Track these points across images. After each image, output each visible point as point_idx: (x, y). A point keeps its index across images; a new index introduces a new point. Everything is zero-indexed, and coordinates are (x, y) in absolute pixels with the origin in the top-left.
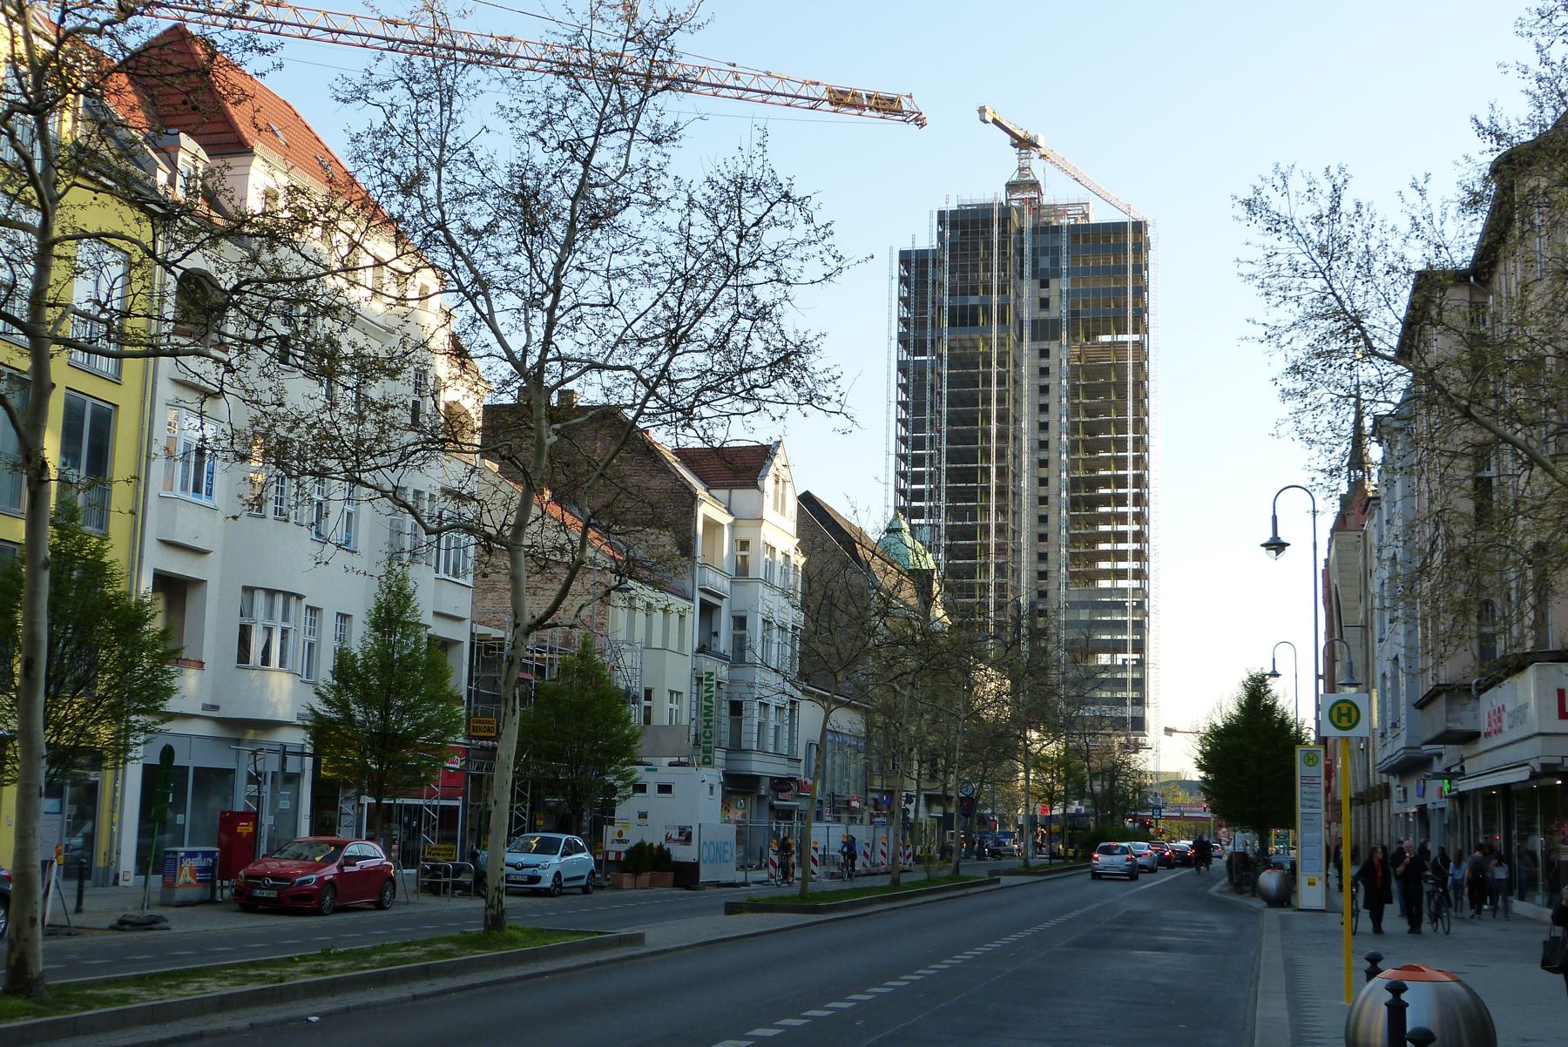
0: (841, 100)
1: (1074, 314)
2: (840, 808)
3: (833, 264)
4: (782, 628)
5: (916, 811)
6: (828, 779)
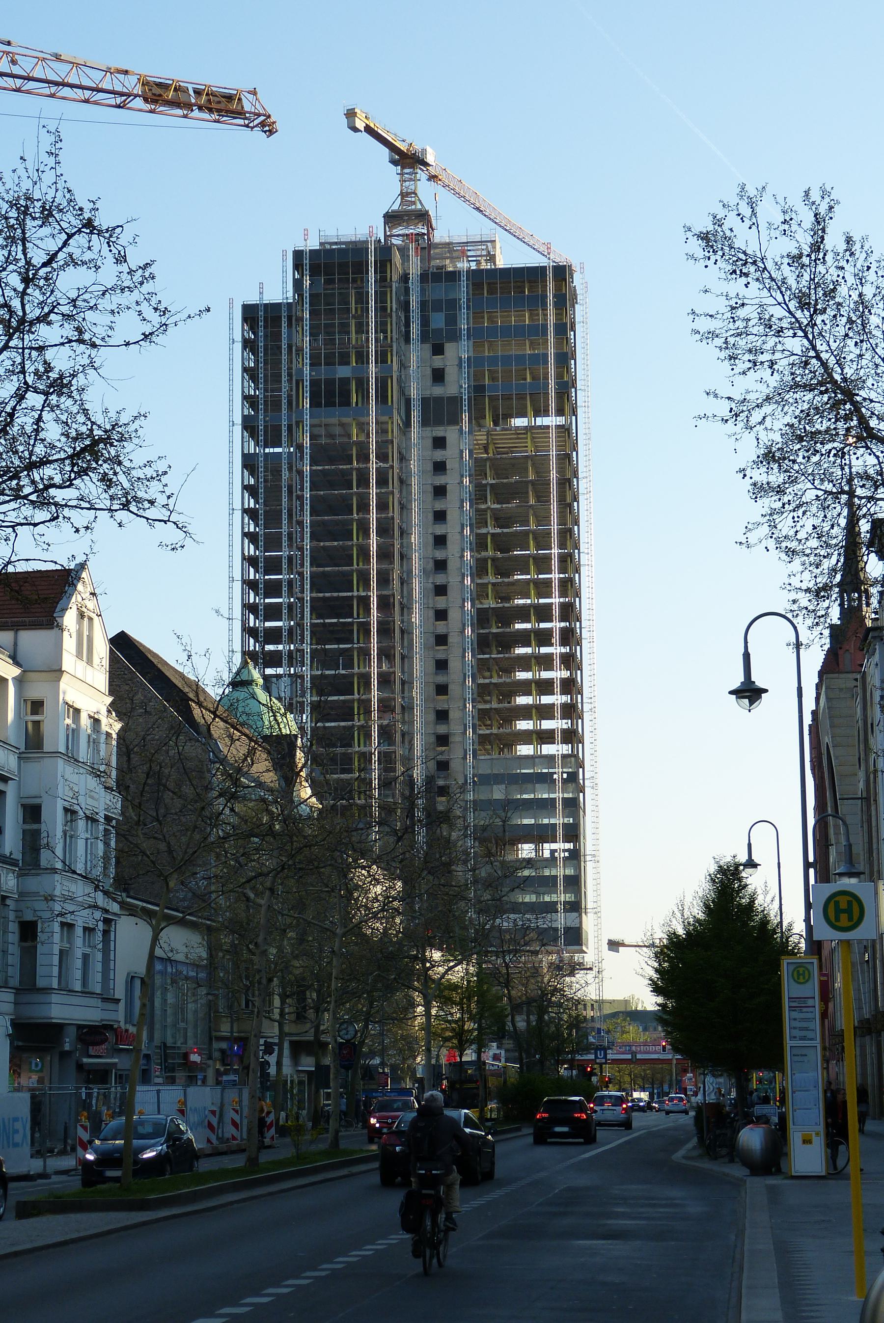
0: (160, 95)
1: (478, 390)
2: (176, 1067)
3: (155, 318)
4: (91, 819)
5: (279, 1064)
6: (157, 1026)
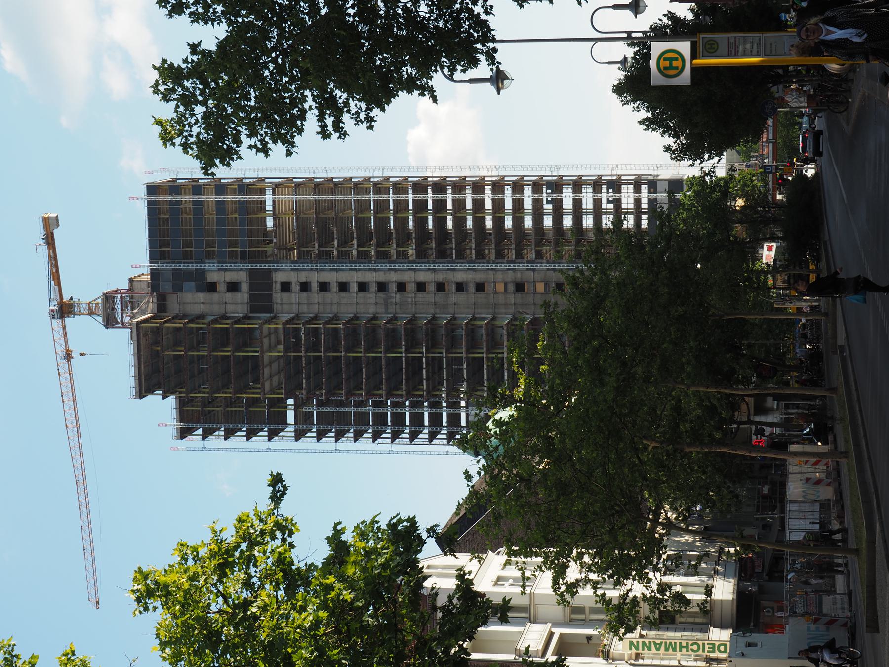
1: (245, 256)
5: (771, 425)
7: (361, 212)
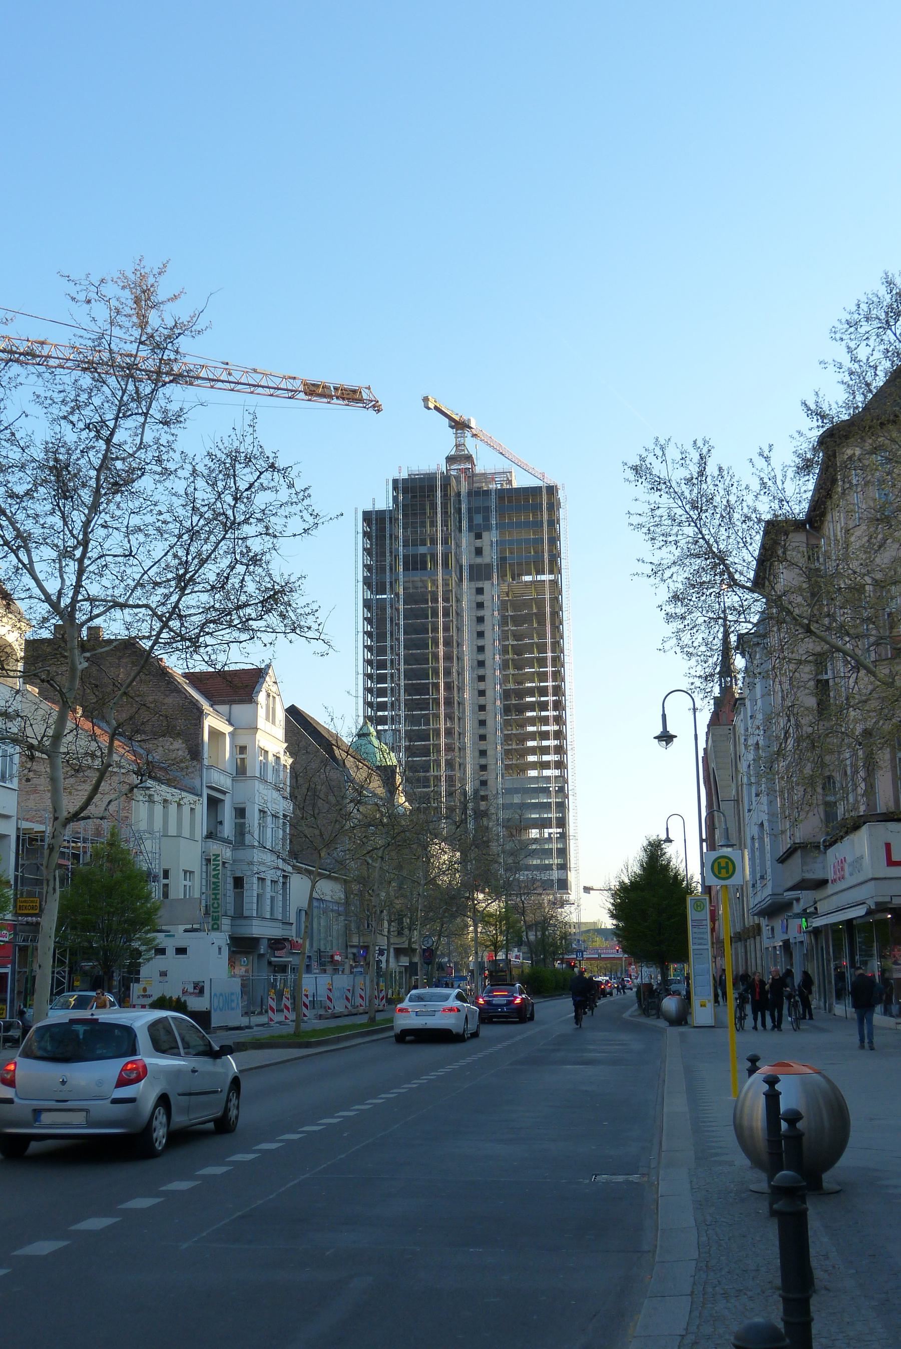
1: (503, 559)
5: (388, 961)
7: (537, 648)
